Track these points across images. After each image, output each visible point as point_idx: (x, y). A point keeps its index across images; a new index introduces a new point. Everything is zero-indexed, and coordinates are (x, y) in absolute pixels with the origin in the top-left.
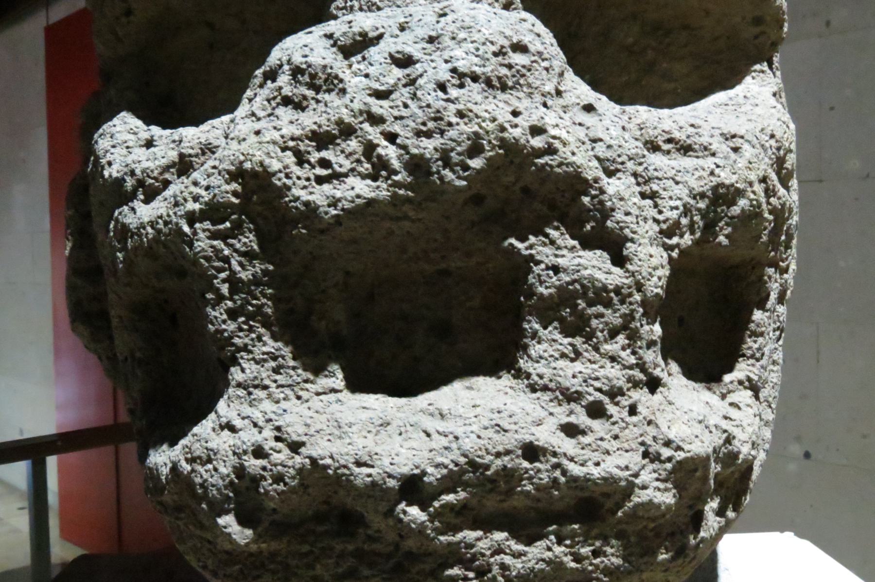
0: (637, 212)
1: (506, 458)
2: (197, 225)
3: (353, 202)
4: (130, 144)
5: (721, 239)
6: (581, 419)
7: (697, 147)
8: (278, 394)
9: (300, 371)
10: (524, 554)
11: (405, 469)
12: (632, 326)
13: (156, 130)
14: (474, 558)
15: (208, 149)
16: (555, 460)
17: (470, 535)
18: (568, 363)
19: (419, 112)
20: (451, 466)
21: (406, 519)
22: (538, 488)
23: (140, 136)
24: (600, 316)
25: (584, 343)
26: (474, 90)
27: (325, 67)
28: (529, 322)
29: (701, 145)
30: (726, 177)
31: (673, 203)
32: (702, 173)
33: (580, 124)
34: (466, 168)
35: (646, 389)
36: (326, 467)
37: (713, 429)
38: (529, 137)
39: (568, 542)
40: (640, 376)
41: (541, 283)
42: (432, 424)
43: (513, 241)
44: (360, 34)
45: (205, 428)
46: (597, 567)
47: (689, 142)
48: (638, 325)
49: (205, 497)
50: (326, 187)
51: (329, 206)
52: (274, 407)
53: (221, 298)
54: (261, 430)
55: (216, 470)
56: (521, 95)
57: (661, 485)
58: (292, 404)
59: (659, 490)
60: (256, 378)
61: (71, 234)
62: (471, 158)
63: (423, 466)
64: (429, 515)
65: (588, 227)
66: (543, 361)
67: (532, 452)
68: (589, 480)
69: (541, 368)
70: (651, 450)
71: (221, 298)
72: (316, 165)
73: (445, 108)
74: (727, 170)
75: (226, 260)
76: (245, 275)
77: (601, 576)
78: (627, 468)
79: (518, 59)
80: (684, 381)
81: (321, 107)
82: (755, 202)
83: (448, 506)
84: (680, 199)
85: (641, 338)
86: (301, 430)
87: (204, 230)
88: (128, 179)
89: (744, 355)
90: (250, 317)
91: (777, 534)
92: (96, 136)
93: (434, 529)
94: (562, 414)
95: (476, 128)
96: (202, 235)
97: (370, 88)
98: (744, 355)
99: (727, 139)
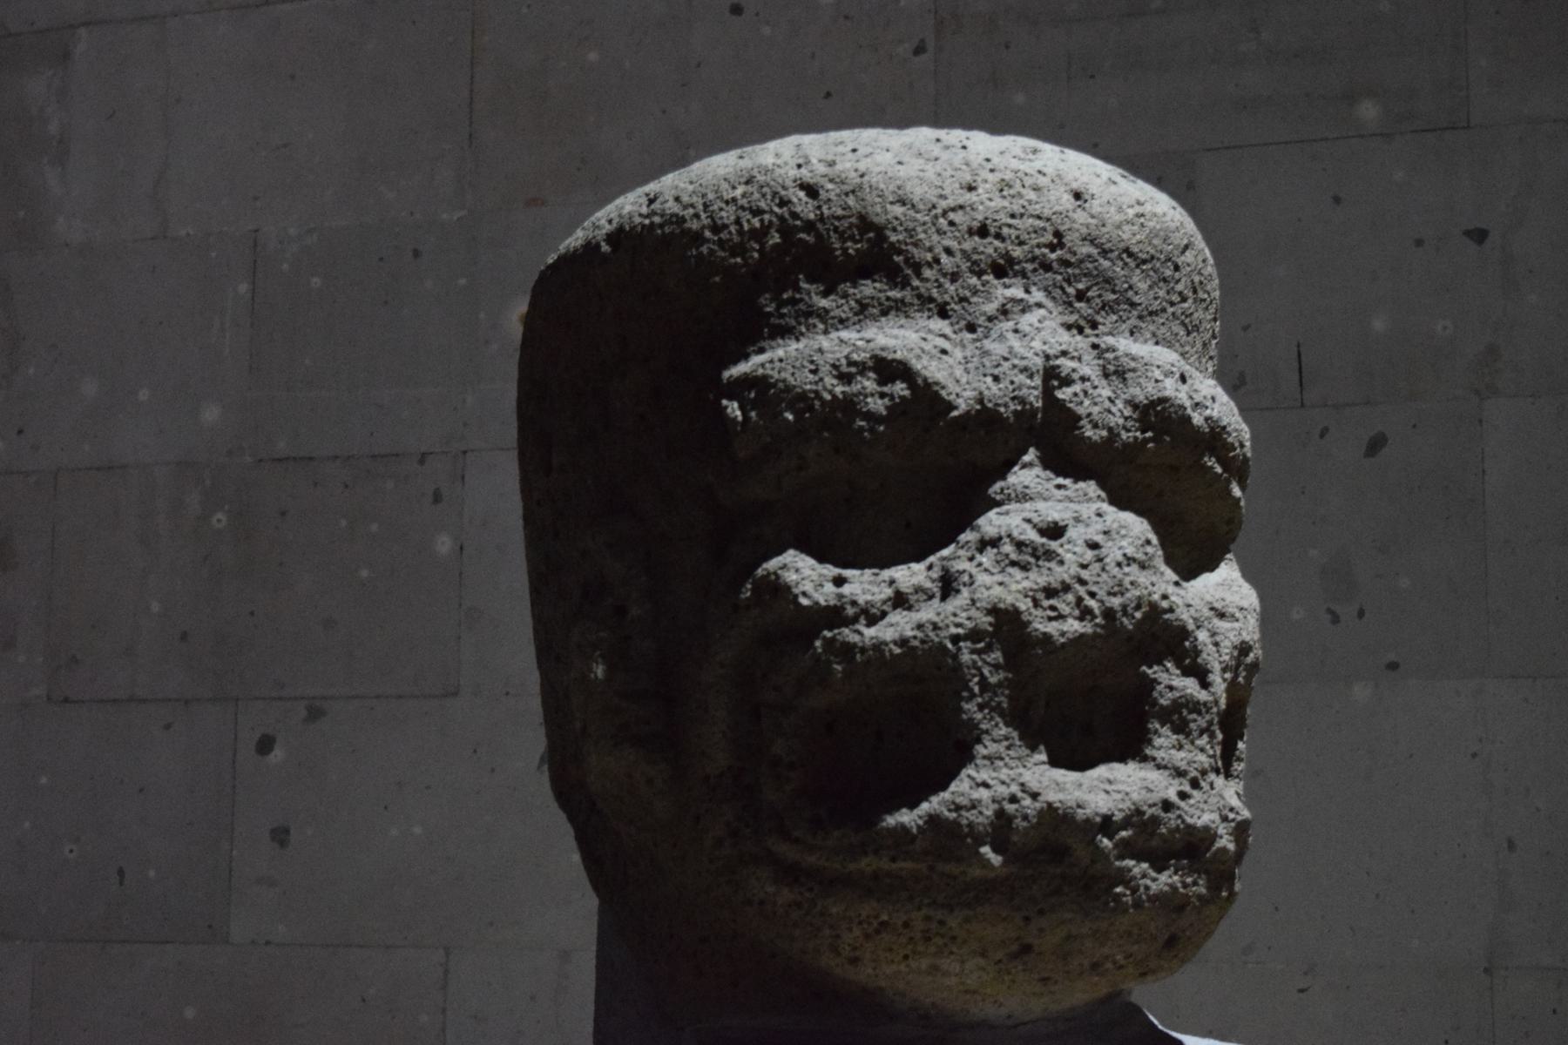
1: (1154, 809)
2: (962, 644)
8: (1013, 763)
9: (1023, 748)
11: (1104, 810)
17: (1131, 863)
19: (1109, 580)
24: (1195, 721)
26: (1134, 568)
28: (1152, 723)
36: (1058, 809)
41: (1162, 696)
43: (1144, 668)
46: (1194, 892)
50: (1054, 624)
53: (973, 696)
54: (1008, 786)
55: (981, 813)
60: (996, 753)
76: (993, 680)
83: (1123, 839)
87: (966, 648)
90: (992, 710)
96: (965, 651)
97: (1077, 562)
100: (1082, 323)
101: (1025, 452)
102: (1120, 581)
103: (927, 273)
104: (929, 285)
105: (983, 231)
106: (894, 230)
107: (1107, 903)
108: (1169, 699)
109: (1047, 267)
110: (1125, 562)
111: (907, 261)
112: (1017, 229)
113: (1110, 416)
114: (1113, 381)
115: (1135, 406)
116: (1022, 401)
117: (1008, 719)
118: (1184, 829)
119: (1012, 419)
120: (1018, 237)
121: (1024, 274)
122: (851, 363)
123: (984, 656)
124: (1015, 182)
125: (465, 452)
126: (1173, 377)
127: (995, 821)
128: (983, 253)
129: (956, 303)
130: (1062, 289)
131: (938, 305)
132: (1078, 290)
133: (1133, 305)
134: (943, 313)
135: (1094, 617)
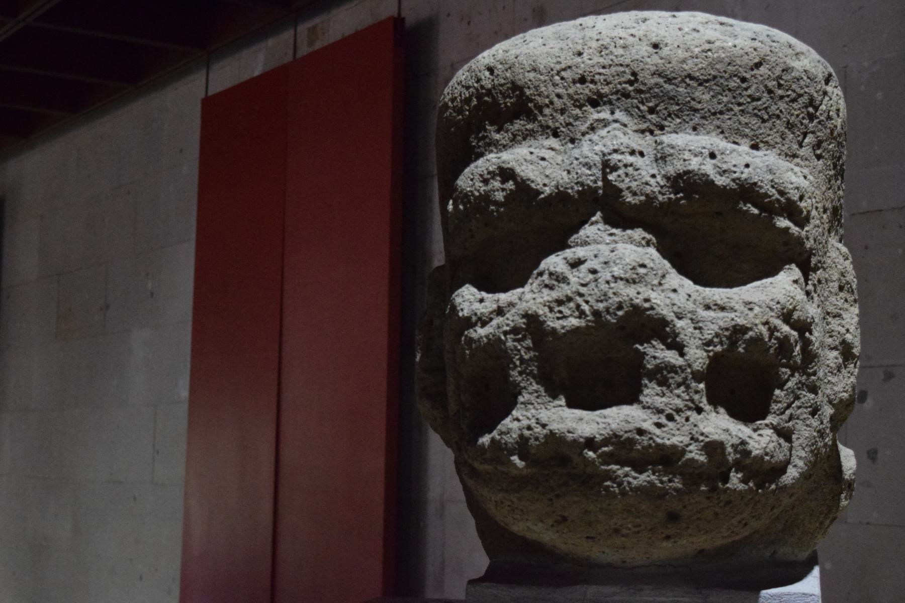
0: (690, 335)
2: (508, 336)
4: (472, 300)
5: (741, 350)
6: (663, 420)
7: (728, 308)
9: (547, 398)
10: (638, 478)
13: (484, 294)
15: (511, 305)
17: (614, 467)
19: (598, 293)
21: (587, 456)
22: (643, 448)
24: (673, 378)
26: (621, 284)
29: (730, 307)
30: (740, 321)
31: (709, 332)
33: (669, 298)
34: (616, 315)
35: (695, 412)
36: (556, 433)
37: (734, 437)
39: (657, 474)
40: (692, 405)
41: (649, 363)
43: (638, 346)
45: (507, 421)
46: (670, 487)
50: (561, 322)
53: (516, 366)
55: (511, 436)
56: (642, 285)
57: (699, 452)
58: (544, 411)
60: (529, 400)
63: (595, 434)
67: (641, 432)
68: (664, 446)
69: (647, 399)
71: (516, 366)
72: (580, 311)
74: (742, 318)
75: (519, 351)
76: (526, 357)
78: (682, 442)
79: (642, 271)
80: (727, 417)
81: (560, 290)
82: (758, 334)
83: (604, 452)
89: (770, 412)
90: (528, 374)
92: (453, 296)
93: (599, 462)
94: (655, 418)
95: (620, 299)
96: (510, 340)
97: (579, 283)
98: (770, 412)
100: (652, 127)
101: (594, 215)
102: (605, 292)
103: (547, 111)
104: (546, 119)
105: (582, 80)
106: (529, 88)
108: (653, 365)
109: (627, 95)
110: (613, 280)
111: (535, 106)
112: (604, 75)
114: (659, 163)
115: (668, 178)
116: (582, 184)
117: (538, 380)
118: (655, 446)
119: (576, 196)
120: (605, 80)
121: (610, 103)
122: (489, 173)
123: (522, 343)
124: (610, 45)
126: (702, 156)
127: (519, 441)
128: (582, 93)
129: (564, 127)
130: (638, 108)
131: (552, 130)
132: (649, 107)
133: (696, 110)
134: (556, 135)
135: (587, 316)
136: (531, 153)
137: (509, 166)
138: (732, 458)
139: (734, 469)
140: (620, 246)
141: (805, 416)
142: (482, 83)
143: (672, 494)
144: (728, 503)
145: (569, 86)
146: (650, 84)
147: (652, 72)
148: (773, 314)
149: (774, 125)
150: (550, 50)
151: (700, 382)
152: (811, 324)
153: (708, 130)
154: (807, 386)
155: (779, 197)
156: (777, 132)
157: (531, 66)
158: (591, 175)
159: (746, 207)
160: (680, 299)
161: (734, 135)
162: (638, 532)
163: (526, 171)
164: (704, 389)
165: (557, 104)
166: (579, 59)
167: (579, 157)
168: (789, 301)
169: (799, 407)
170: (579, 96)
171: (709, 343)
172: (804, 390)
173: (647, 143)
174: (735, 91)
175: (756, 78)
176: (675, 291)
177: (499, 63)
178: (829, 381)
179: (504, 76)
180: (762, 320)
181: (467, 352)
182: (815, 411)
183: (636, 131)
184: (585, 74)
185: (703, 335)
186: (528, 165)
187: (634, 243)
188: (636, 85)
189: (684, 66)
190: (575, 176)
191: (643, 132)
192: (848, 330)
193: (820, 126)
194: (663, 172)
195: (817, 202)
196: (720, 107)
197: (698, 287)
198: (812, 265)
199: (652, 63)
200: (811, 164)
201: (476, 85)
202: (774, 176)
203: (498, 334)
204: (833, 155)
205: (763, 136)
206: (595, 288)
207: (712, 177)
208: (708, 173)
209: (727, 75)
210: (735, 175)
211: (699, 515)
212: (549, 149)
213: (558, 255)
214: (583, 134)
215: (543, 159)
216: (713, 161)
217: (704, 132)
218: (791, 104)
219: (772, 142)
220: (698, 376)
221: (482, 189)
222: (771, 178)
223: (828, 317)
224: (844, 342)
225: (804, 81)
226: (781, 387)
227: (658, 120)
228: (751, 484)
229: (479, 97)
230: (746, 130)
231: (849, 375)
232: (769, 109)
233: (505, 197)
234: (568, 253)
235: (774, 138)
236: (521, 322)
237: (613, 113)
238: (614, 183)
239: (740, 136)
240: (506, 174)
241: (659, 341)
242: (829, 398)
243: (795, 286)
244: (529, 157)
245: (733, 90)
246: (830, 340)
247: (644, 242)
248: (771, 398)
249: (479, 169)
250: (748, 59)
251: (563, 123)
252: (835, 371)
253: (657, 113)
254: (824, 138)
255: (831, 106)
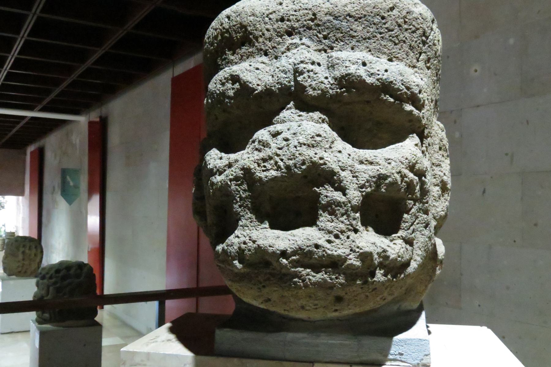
0: (350, 181)
1: (310, 248)
2: (232, 182)
3: (271, 177)
4: (216, 158)
5: (383, 190)
6: (332, 238)
8: (251, 228)
9: (257, 222)
11: (282, 248)
12: (348, 213)
13: (223, 154)
14: (301, 276)
15: (237, 161)
16: (323, 249)
17: (300, 269)
18: (330, 223)
19: (289, 154)
20: (294, 248)
21: (282, 262)
22: (319, 257)
23: (218, 156)
24: (339, 210)
25: (335, 217)
27: (266, 141)
28: (320, 211)
30: (383, 171)
31: (362, 179)
32: (374, 170)
33: (336, 156)
34: (301, 168)
35: (353, 232)
36: (262, 247)
37: (379, 247)
38: (319, 160)
39: (328, 274)
41: (323, 200)
42: (290, 238)
43: (315, 188)
44: (277, 131)
45: (232, 237)
47: (372, 161)
48: (350, 213)
49: (230, 256)
50: (265, 173)
51: (265, 178)
52: (250, 232)
53: (237, 202)
55: (233, 248)
56: (318, 148)
57: (356, 259)
59: (355, 261)
60: (245, 224)
61: (195, 185)
62: (302, 166)
63: (287, 248)
64: (288, 262)
65: (336, 185)
66: (323, 222)
67: (317, 246)
68: (333, 255)
69: (322, 224)
70: (353, 249)
71: (237, 202)
73: (296, 153)
74: (384, 170)
75: (239, 192)
76: (243, 196)
77: (338, 285)
78: (344, 253)
79: (318, 139)
80: (374, 233)
82: (394, 179)
83: (293, 260)
84: (365, 178)
85: (351, 217)
86: (256, 237)
87: (234, 184)
88: (214, 169)
89: (401, 229)
90: (245, 207)
91: (479, 327)
92: (206, 155)
94: (327, 237)
95: (304, 158)
97: (277, 147)
98: (401, 229)
99: (387, 160)
100: (326, 48)
101: (289, 104)
103: (261, 40)
104: (260, 44)
105: (282, 20)
106: (250, 26)
107: (291, 285)
108: (326, 201)
109: (310, 28)
111: (254, 37)
112: (296, 16)
113: (322, 84)
115: (336, 79)
116: (281, 84)
117: (251, 211)
119: (277, 91)
120: (296, 19)
121: (300, 33)
122: (225, 79)
125: (461, 109)
126: (357, 64)
128: (282, 28)
129: (271, 49)
130: (317, 36)
132: (323, 35)
133: (353, 37)
134: (266, 54)
136: (250, 65)
137: (236, 74)
138: (378, 261)
139: (378, 268)
140: (304, 123)
141: (421, 229)
142: (224, 26)
143: (338, 286)
144: (375, 289)
145: (274, 23)
146: (324, 20)
147: (326, 13)
148: (403, 166)
149: (402, 47)
150: (263, 2)
151: (356, 213)
152: (426, 171)
153: (361, 49)
154: (423, 210)
155: (406, 91)
156: (404, 51)
157: (251, 13)
158: (286, 78)
159: (386, 97)
160: (343, 157)
161: (378, 53)
162: (316, 309)
163: (246, 76)
164: (359, 217)
165: (267, 35)
166: (280, 7)
167: (279, 66)
168: (413, 157)
169: (418, 224)
170: (280, 30)
171: (363, 186)
172: (420, 213)
173: (322, 57)
174: (378, 24)
175: (391, 17)
176: (340, 152)
177: (233, 13)
178: (434, 205)
179: (236, 20)
180: (396, 170)
181: (211, 191)
182: (427, 226)
183: (316, 50)
184: (284, 15)
185: (359, 181)
186: (248, 72)
187: (314, 121)
188: (315, 21)
189: (346, 8)
190: (277, 79)
191: (320, 51)
192: (444, 174)
193: (429, 49)
194: (332, 75)
195: (428, 95)
196: (368, 34)
197: (355, 149)
198: (425, 135)
199: (326, 7)
200: (424, 72)
201: (220, 27)
202: (403, 77)
203: (226, 181)
204: (436, 67)
205: (395, 53)
206: (287, 151)
207: (364, 77)
208: (361, 75)
209: (372, 15)
210: (379, 77)
211: (356, 298)
212: (261, 63)
213: (265, 129)
214: (283, 54)
215: (257, 69)
216: (365, 68)
217: (359, 50)
218: (412, 34)
219: (401, 58)
220: (355, 209)
221: (221, 89)
222: (402, 79)
223: (433, 166)
224: (442, 181)
225: (420, 20)
226: (408, 213)
227: (329, 43)
228: (389, 277)
229: (222, 34)
230: (385, 50)
231: (445, 201)
232: (399, 37)
233: (234, 93)
234: (272, 128)
235: (402, 55)
236: (240, 173)
237: (301, 39)
238: (301, 82)
239: (381, 53)
240: (235, 79)
241: (329, 186)
242: (434, 216)
243: (416, 147)
244: (249, 68)
245: (377, 24)
246: (435, 180)
247: (320, 121)
248: (401, 220)
249: (220, 77)
250: (386, 5)
251: (270, 46)
252: (438, 199)
253: (329, 39)
254: (432, 56)
255: (435, 37)
